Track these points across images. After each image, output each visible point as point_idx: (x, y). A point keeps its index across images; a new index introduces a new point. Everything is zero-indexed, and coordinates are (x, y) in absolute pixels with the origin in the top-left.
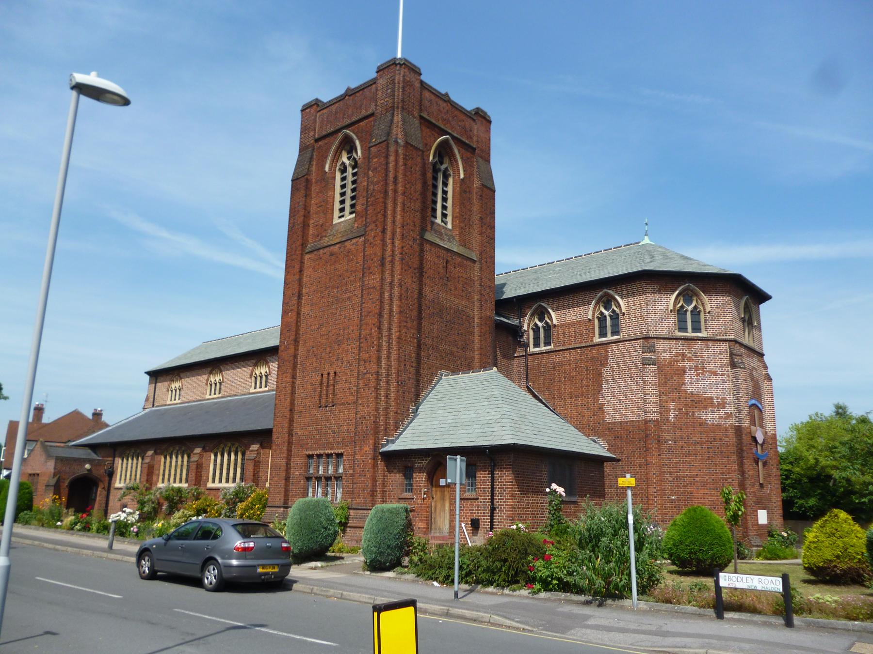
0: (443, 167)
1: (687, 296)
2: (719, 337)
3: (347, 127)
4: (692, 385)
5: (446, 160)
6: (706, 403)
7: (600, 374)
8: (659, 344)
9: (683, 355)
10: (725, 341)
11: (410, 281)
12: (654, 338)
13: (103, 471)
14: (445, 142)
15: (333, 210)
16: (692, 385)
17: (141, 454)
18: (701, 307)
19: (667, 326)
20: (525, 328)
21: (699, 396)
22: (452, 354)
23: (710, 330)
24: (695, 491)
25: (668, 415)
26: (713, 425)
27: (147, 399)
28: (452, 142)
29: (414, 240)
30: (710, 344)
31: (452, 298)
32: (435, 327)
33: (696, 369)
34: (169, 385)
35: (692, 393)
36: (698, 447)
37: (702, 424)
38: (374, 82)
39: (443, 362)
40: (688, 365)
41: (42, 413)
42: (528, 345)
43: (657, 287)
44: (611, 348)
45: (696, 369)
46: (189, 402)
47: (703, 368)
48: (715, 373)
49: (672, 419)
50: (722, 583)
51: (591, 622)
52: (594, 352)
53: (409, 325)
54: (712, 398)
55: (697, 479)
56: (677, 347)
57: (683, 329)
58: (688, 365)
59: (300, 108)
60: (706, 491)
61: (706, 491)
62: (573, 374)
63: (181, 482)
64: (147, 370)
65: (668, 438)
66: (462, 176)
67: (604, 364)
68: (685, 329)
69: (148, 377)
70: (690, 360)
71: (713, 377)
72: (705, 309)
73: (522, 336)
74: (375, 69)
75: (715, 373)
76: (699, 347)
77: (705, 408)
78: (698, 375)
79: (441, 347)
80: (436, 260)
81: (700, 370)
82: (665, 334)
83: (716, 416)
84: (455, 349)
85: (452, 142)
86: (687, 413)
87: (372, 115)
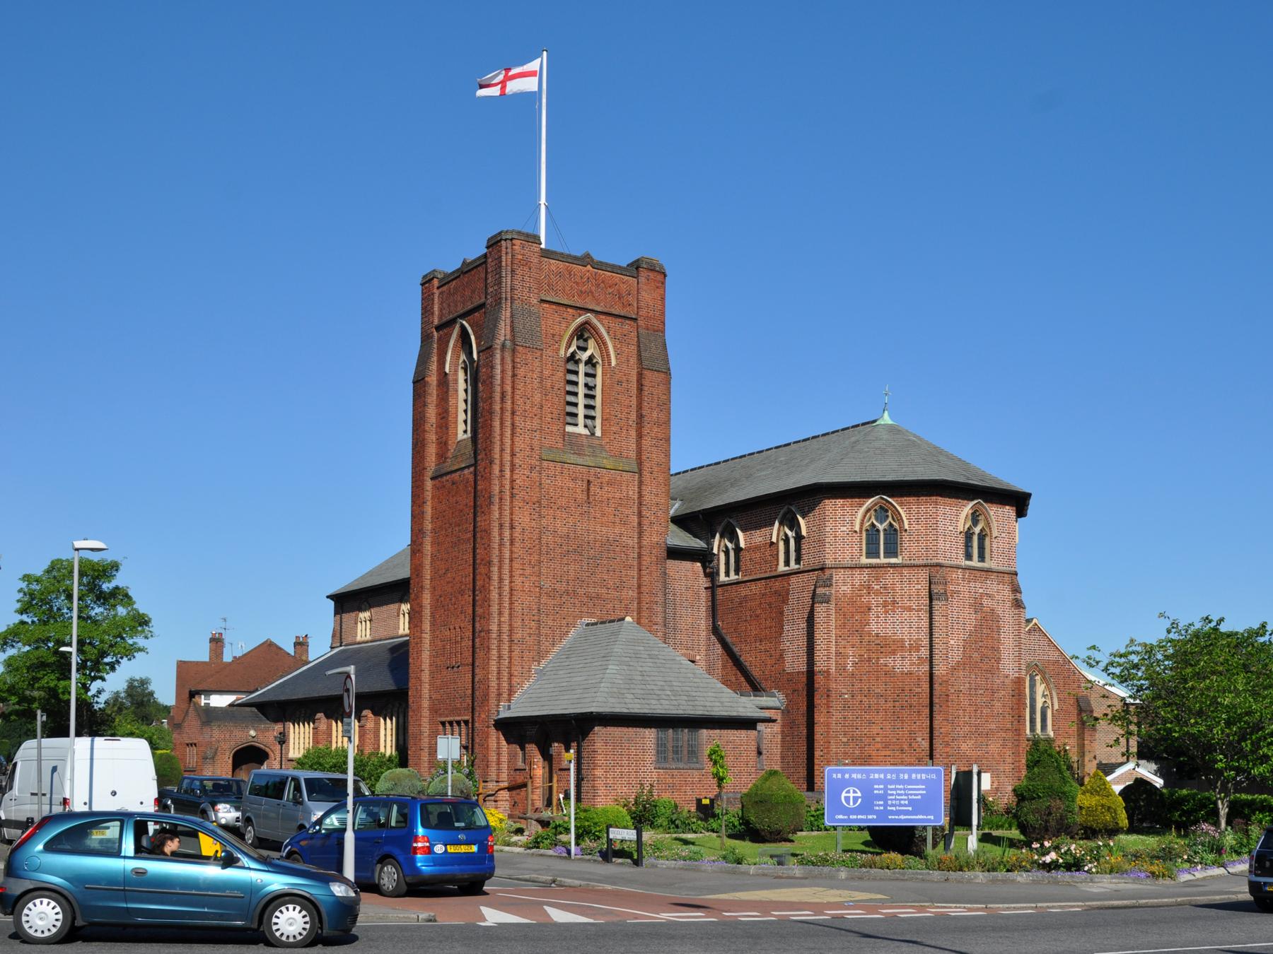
0: (585, 356)
2: (917, 562)
3: (463, 316)
4: (878, 625)
5: (591, 343)
7: (782, 613)
10: (925, 566)
11: (527, 519)
13: (272, 738)
14: (587, 323)
15: (456, 422)
17: (309, 718)
20: (715, 551)
21: (885, 638)
22: (598, 597)
24: (874, 753)
27: (334, 636)
28: (595, 321)
29: (532, 468)
30: (905, 571)
31: (598, 528)
32: (572, 567)
33: (885, 604)
34: (357, 616)
35: (877, 635)
36: (882, 701)
38: (485, 256)
39: (585, 609)
40: (874, 601)
41: (222, 647)
42: (718, 574)
44: (793, 579)
45: (885, 604)
46: (72, 780)
47: (894, 602)
48: (910, 609)
49: (850, 668)
50: (611, 836)
51: (523, 866)
52: (777, 584)
53: (528, 572)
54: (903, 641)
55: (878, 739)
56: (860, 577)
57: (873, 552)
58: (874, 601)
59: (420, 280)
60: (888, 753)
62: (758, 612)
64: (332, 591)
65: (844, 691)
69: (332, 603)
70: (878, 593)
73: (711, 562)
74: (485, 244)
76: (890, 578)
77: (894, 652)
79: (581, 591)
80: (571, 485)
81: (890, 606)
82: (847, 561)
83: (907, 662)
84: (604, 591)
86: (869, 660)
87: (483, 306)
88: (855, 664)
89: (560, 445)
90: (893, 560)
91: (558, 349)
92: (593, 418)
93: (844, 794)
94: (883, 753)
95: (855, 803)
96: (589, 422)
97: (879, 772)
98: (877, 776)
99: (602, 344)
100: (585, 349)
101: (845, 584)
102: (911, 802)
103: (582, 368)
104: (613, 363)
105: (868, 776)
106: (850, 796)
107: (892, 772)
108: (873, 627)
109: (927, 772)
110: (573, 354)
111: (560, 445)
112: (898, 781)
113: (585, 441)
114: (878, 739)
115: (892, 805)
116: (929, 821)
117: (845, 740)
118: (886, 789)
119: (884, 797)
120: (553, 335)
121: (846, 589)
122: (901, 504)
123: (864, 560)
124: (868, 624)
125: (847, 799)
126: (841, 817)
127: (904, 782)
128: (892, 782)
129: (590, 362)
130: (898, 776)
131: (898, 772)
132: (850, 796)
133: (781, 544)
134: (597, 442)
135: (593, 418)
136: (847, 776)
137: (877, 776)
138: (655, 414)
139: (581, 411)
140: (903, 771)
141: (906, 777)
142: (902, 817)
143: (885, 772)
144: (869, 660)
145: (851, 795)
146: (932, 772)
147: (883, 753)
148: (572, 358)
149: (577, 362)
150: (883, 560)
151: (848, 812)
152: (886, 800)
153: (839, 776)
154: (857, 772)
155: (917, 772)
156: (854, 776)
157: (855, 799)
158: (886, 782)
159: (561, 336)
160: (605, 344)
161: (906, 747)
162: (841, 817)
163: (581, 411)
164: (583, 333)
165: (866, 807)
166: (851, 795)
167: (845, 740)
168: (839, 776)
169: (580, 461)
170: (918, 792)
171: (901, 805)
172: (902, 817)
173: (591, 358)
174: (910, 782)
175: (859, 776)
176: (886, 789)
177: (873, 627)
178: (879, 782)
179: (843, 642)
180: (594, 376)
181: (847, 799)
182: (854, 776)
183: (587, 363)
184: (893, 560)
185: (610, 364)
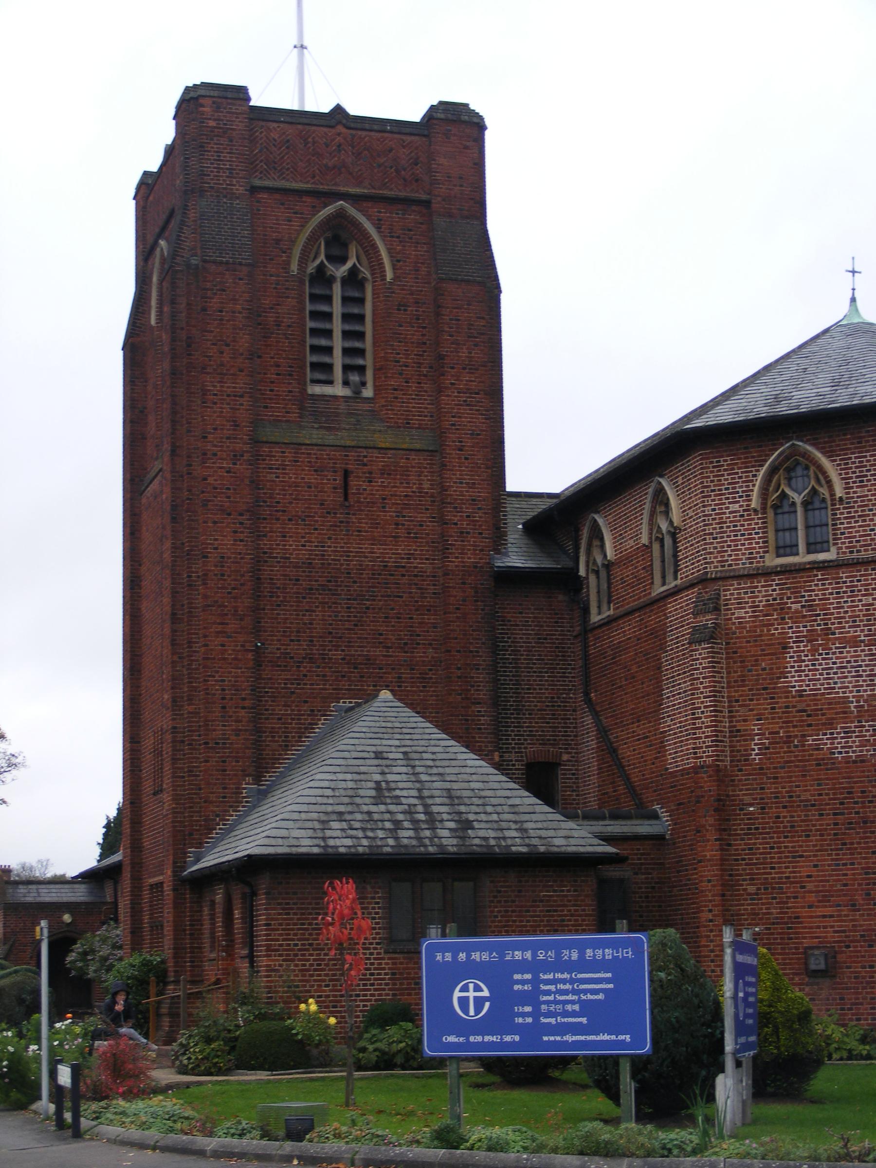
0: (342, 270)
1: (790, 466)
4: (801, 675)
6: (824, 712)
8: (731, 592)
9: (783, 609)
12: (716, 579)
14: (341, 214)
16: (801, 675)
18: (824, 491)
19: (749, 547)
20: (582, 572)
23: (844, 543)
25: (748, 750)
26: (847, 760)
28: (352, 211)
29: (236, 457)
33: (811, 637)
37: (825, 763)
43: (726, 461)
44: (672, 606)
45: (811, 637)
47: (827, 632)
48: (855, 642)
49: (755, 756)
54: (845, 701)
56: (765, 592)
60: (829, 911)
61: (829, 911)
62: (634, 669)
63: (563, 804)
65: (747, 799)
66: (389, 276)
67: (662, 647)
68: (791, 549)
70: (797, 617)
71: (849, 652)
72: (832, 495)
75: (855, 642)
76: (818, 588)
77: (830, 724)
78: (814, 651)
81: (821, 639)
82: (743, 565)
85: (352, 211)
86: (788, 740)
88: (764, 748)
89: (293, 416)
90: (822, 556)
91: (288, 263)
92: (361, 369)
93: (457, 994)
94: (820, 912)
95: (478, 1010)
96: (354, 378)
97: (523, 947)
98: (518, 955)
99: (370, 249)
100: (343, 260)
101: (740, 605)
102: (587, 1008)
103: (337, 291)
104: (389, 276)
105: (502, 955)
106: (470, 996)
107: (546, 946)
108: (794, 681)
109: (614, 945)
110: (321, 268)
111: (293, 416)
112: (560, 965)
113: (343, 406)
114: (810, 886)
115: (549, 1014)
116: (621, 1044)
117: (752, 889)
118: (536, 982)
119: (532, 998)
120: (278, 241)
121: (743, 614)
122: (830, 454)
123: (773, 561)
124: (784, 675)
125: (463, 1002)
126: (452, 1039)
127: (569, 967)
128: (547, 966)
129: (353, 279)
130: (558, 955)
131: (558, 947)
132: (470, 996)
133: (656, 547)
134: (366, 407)
135: (361, 369)
136: (462, 956)
137: (518, 955)
138: (464, 353)
139: (338, 360)
140: (570, 945)
141: (575, 956)
142: (569, 1038)
143: (534, 947)
144: (788, 740)
145: (471, 994)
146: (624, 944)
147: (820, 912)
148: (321, 277)
149: (330, 280)
150: (803, 558)
151: (466, 1028)
152: (536, 1004)
153: (448, 957)
154: (481, 948)
155: (596, 945)
156: (476, 956)
157: (479, 1003)
158: (535, 967)
159: (293, 242)
160: (374, 247)
161: (859, 899)
162: (452, 1039)
163: (338, 360)
164: (338, 237)
165: (499, 1019)
166: (471, 994)
167: (752, 889)
168: (528, 955)
169: (330, 439)
170: (598, 986)
171: (566, 1014)
172: (569, 1038)
173: (353, 271)
174: (583, 965)
175: (485, 957)
176: (536, 982)
177: (794, 681)
178: (522, 966)
179: (743, 711)
180: (361, 301)
181: (463, 1002)
182: (476, 956)
183: (345, 282)
184: (822, 556)
185: (383, 278)
